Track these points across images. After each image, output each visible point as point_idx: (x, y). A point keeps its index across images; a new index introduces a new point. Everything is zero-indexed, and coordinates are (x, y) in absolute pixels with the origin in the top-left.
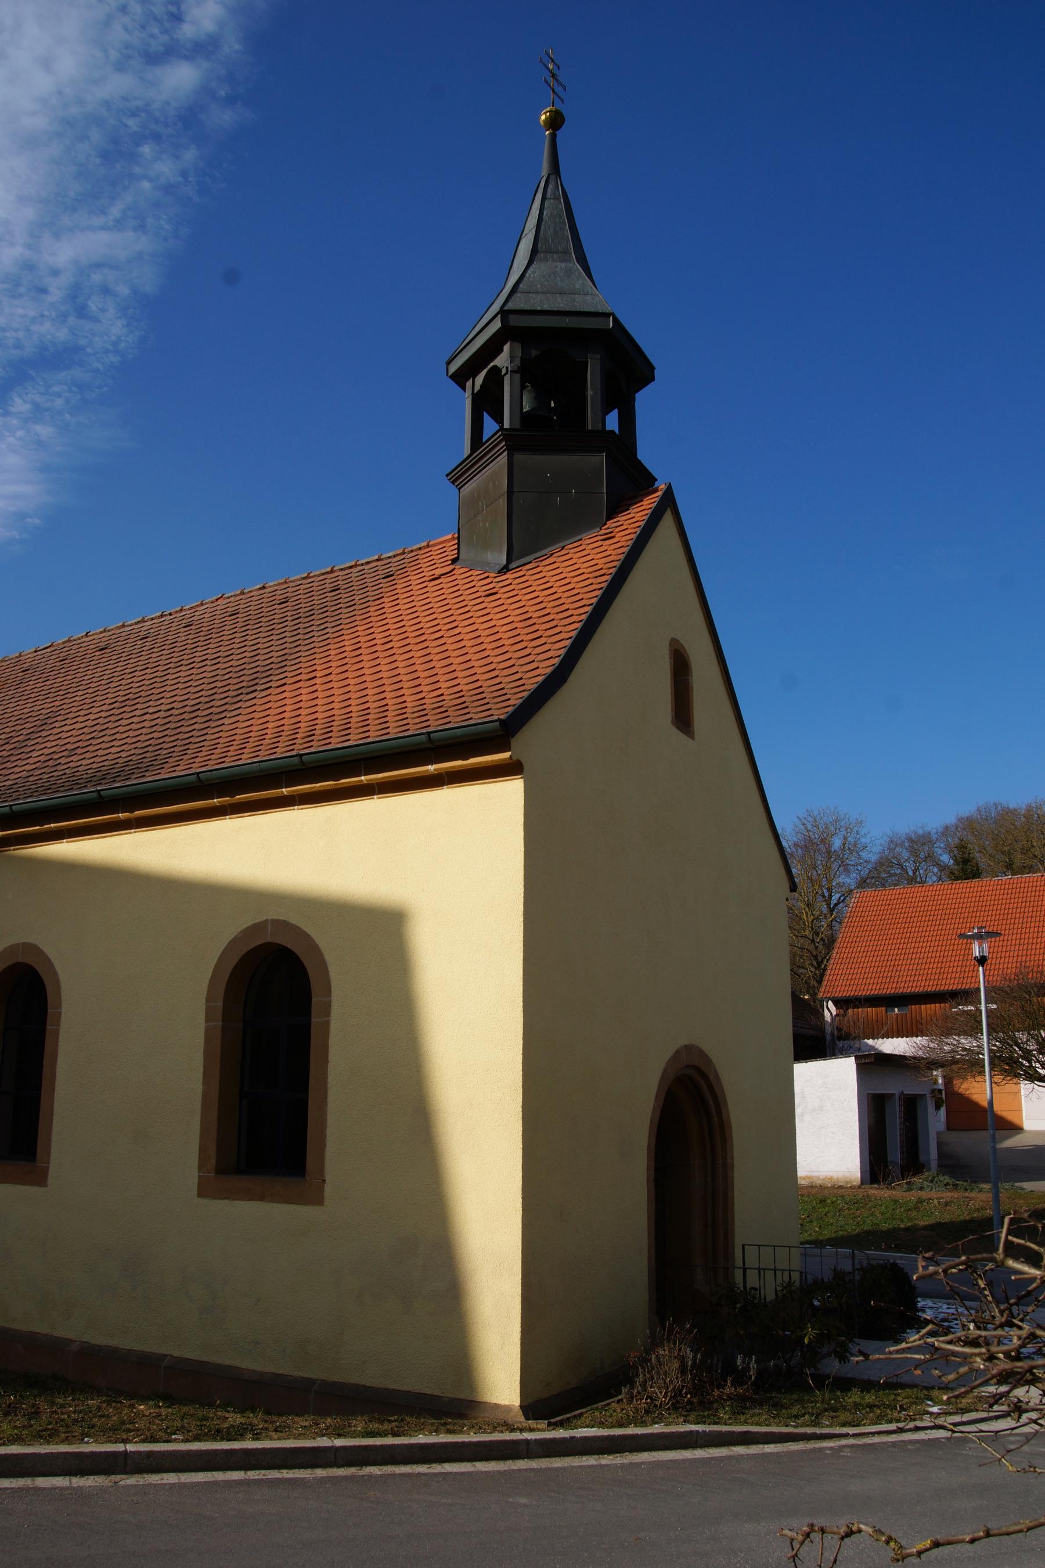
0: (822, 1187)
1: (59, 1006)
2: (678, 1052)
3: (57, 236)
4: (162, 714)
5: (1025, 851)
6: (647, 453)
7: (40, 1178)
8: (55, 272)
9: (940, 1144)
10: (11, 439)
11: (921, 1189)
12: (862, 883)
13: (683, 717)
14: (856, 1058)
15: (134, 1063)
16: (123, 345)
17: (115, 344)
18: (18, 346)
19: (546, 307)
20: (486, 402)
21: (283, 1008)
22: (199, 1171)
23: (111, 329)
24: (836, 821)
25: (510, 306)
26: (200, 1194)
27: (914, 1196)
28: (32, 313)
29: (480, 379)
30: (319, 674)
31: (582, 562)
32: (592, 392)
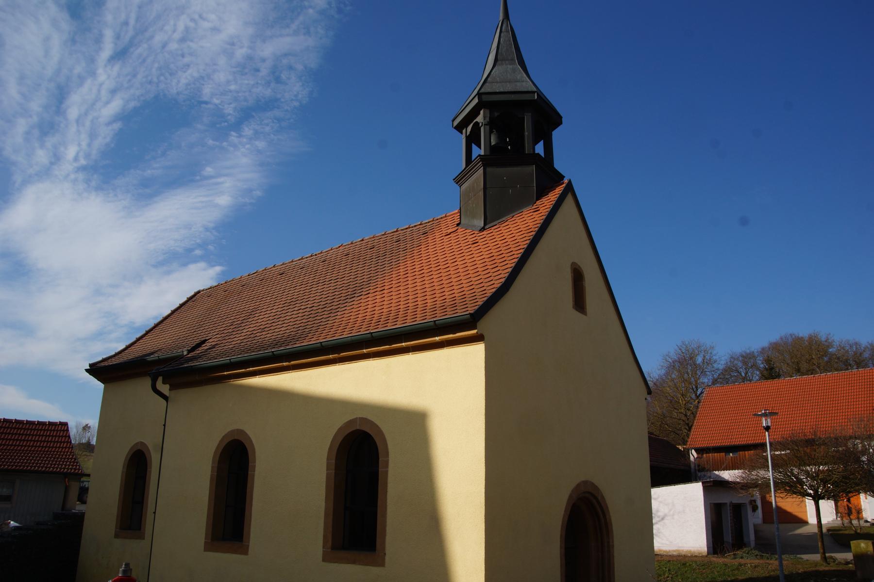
0: (685, 556)
1: (255, 462)
2: (578, 485)
3: (264, 41)
4: (308, 310)
5: (809, 361)
6: (558, 165)
7: (245, 551)
8: (264, 60)
9: (756, 532)
10: (243, 150)
11: (742, 558)
12: (715, 382)
13: (579, 304)
14: (703, 483)
15: (293, 490)
16: (300, 96)
17: (296, 96)
18: (246, 100)
19: (502, 90)
20: (473, 139)
21: (365, 465)
22: (324, 547)
23: (295, 90)
24: (699, 347)
25: (483, 90)
26: (324, 560)
27: (736, 562)
28: (252, 83)
29: (469, 128)
30: (386, 288)
31: (522, 224)
32: (527, 133)
